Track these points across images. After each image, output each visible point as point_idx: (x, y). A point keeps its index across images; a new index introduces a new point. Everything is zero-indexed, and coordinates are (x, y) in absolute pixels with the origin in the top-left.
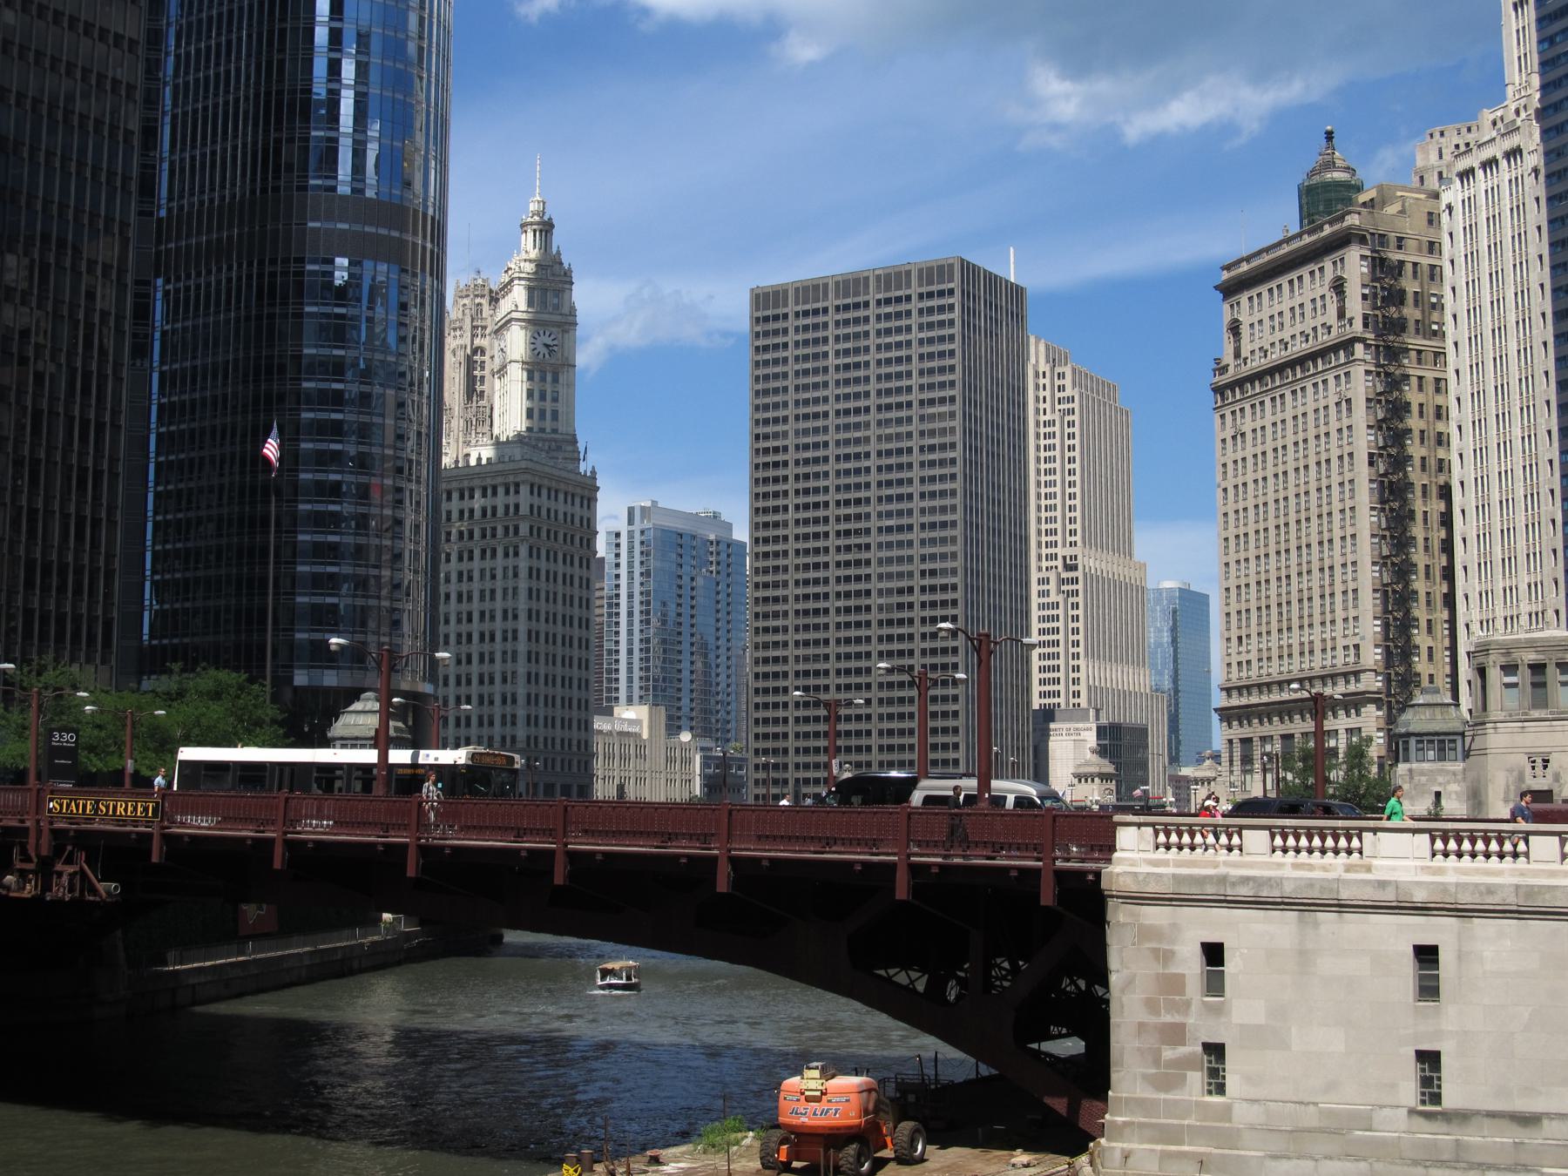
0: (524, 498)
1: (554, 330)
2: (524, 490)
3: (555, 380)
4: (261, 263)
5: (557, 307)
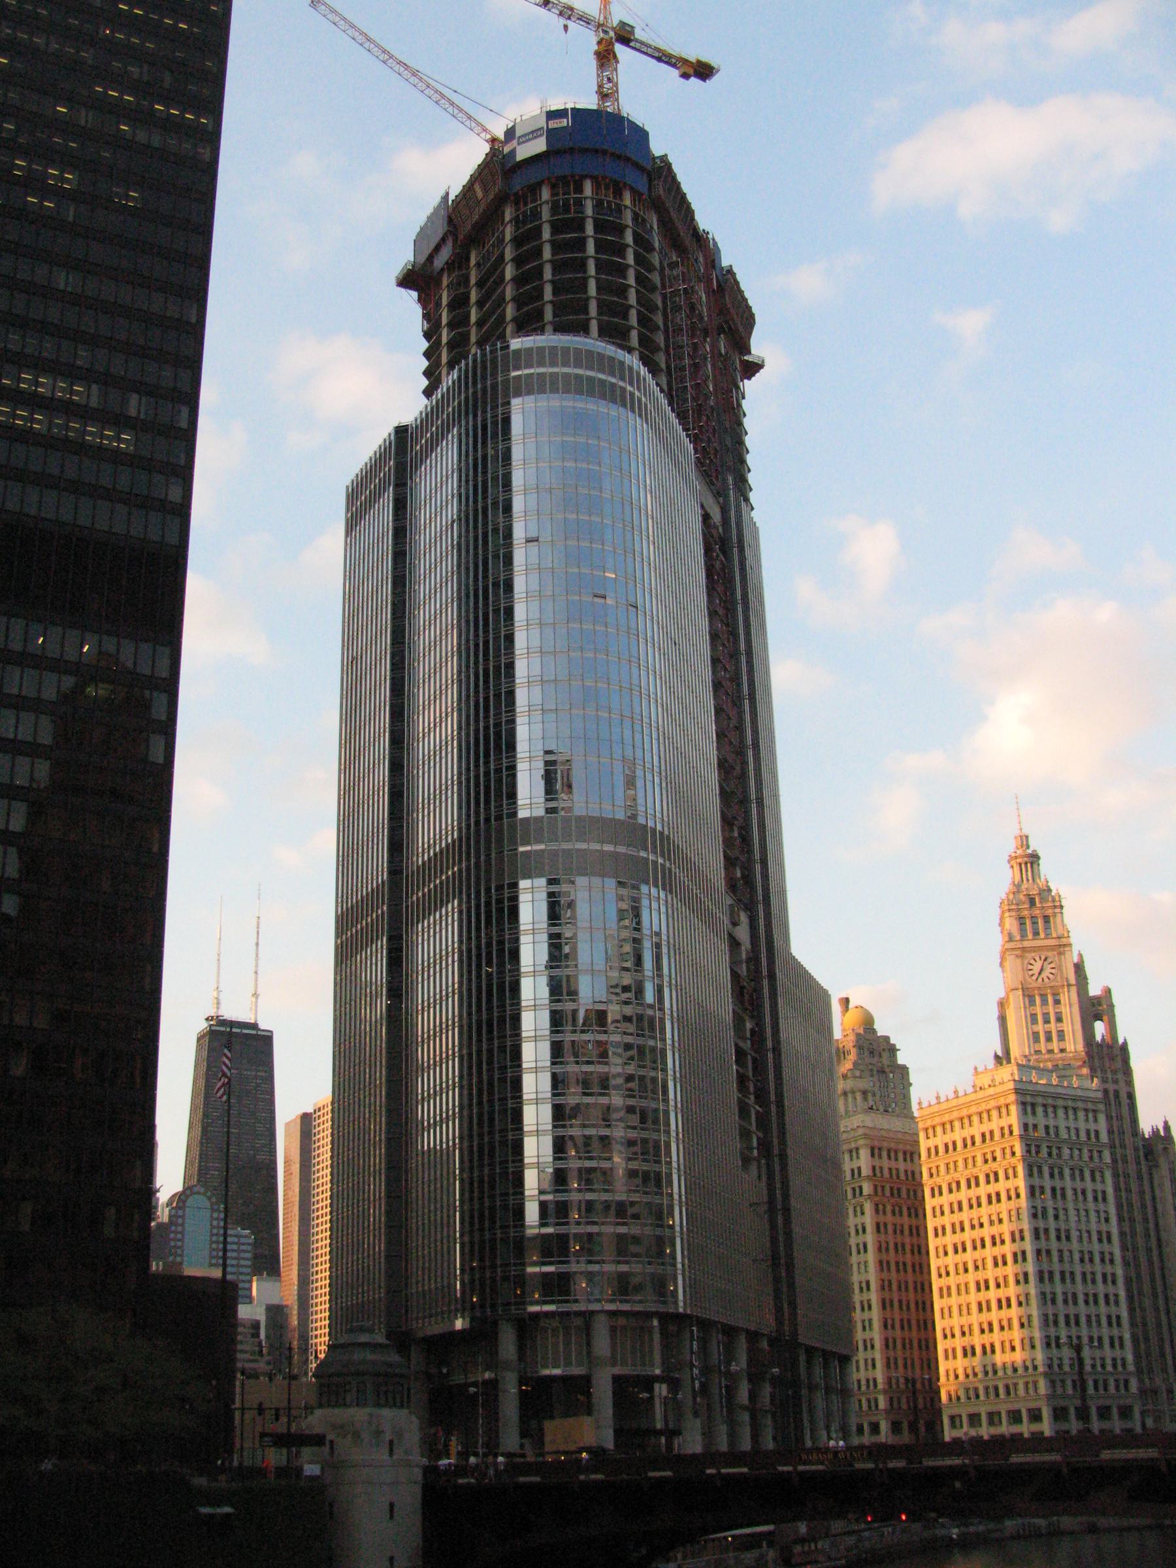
1: (1050, 954)
4: (500, 888)
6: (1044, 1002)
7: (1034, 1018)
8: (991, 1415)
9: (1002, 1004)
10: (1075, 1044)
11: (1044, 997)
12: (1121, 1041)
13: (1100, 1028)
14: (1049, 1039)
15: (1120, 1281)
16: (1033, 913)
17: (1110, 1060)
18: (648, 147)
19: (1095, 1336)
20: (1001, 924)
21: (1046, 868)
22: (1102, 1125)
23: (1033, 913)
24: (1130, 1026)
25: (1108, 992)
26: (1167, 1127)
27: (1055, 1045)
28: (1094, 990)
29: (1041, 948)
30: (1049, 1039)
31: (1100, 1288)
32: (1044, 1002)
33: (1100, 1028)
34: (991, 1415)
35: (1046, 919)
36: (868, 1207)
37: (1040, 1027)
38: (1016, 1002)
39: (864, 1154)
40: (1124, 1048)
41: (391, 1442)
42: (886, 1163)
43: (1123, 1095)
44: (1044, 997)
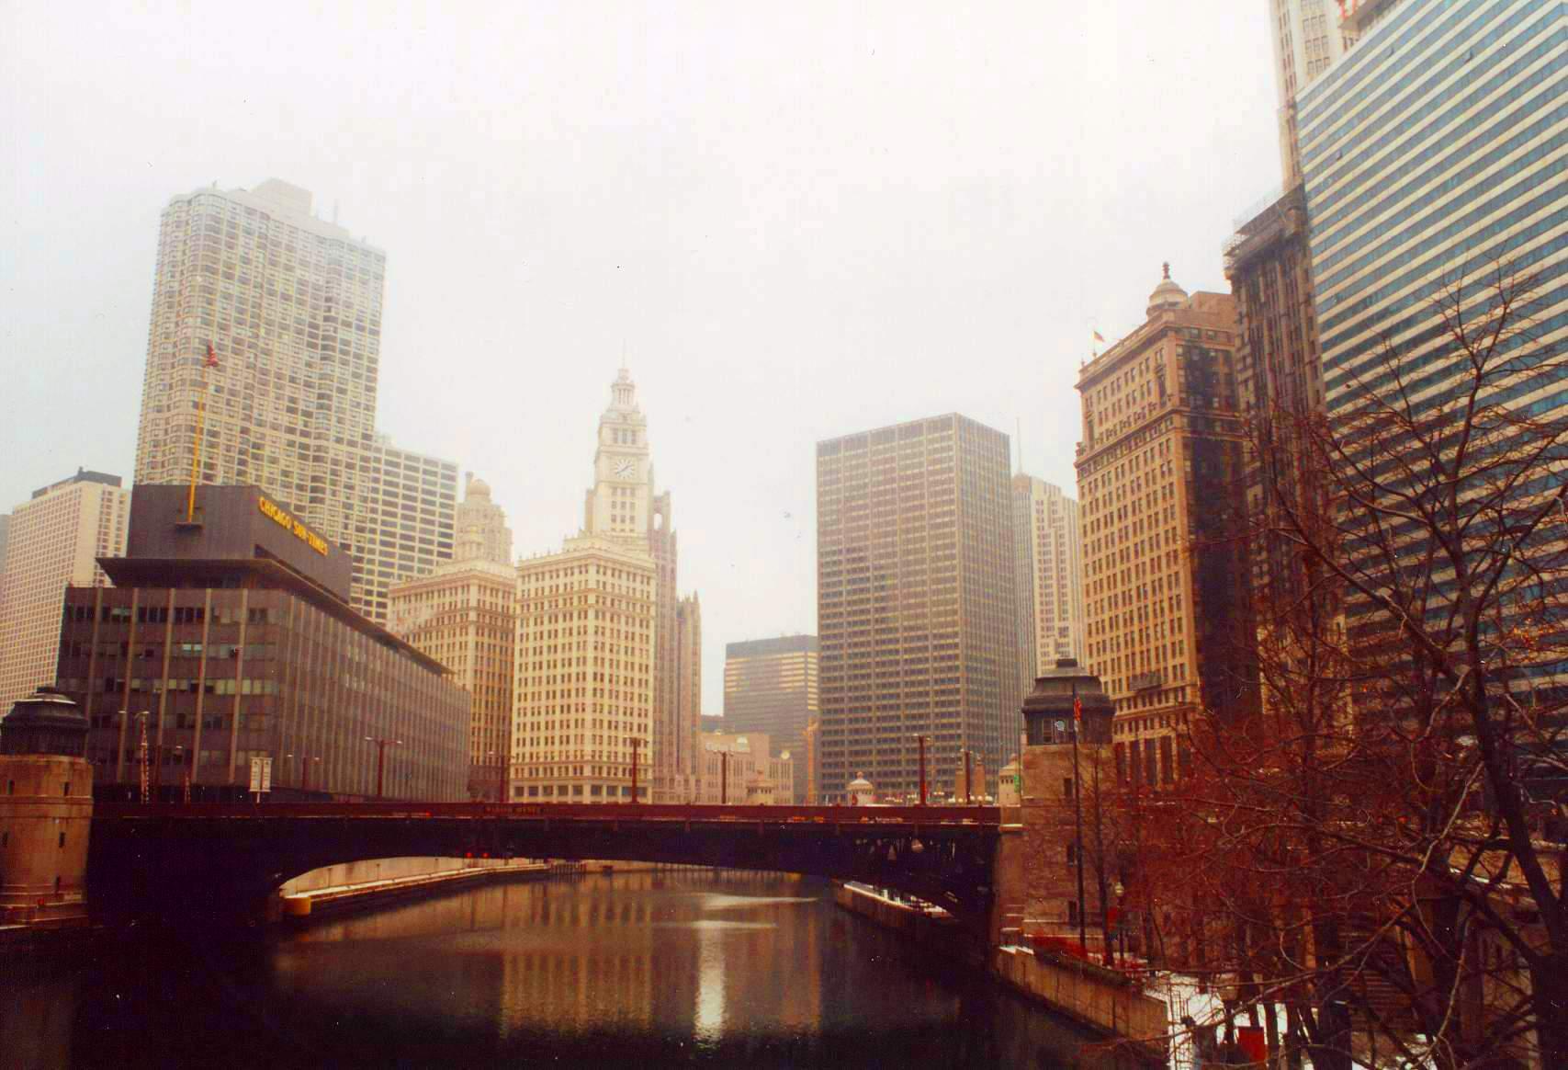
0: (592, 577)
2: (592, 570)
3: (633, 494)
5: (634, 441)
6: (624, 494)
7: (614, 505)
8: (545, 788)
9: (591, 494)
10: (641, 527)
11: (624, 489)
12: (1243, 238)
13: (658, 519)
14: (623, 521)
15: (652, 641)
16: (622, 432)
17: (661, 542)
18: (1281, 202)
19: (618, 921)
20: (600, 432)
21: (640, 399)
22: (652, 588)
23: (622, 432)
24: (681, 523)
25: (667, 494)
26: (696, 598)
27: (627, 526)
28: (658, 492)
29: (625, 454)
30: (623, 504)
31: (637, 675)
32: (624, 494)
33: (658, 519)
34: (545, 788)
35: (634, 433)
36: (472, 630)
37: (618, 512)
38: (604, 491)
39: (474, 589)
40: (673, 537)
41: (67, 785)
42: (488, 599)
43: (669, 567)
44: (624, 489)
